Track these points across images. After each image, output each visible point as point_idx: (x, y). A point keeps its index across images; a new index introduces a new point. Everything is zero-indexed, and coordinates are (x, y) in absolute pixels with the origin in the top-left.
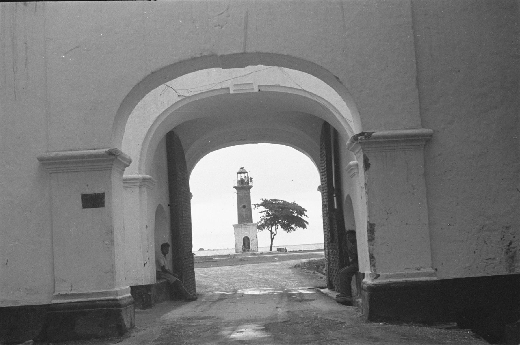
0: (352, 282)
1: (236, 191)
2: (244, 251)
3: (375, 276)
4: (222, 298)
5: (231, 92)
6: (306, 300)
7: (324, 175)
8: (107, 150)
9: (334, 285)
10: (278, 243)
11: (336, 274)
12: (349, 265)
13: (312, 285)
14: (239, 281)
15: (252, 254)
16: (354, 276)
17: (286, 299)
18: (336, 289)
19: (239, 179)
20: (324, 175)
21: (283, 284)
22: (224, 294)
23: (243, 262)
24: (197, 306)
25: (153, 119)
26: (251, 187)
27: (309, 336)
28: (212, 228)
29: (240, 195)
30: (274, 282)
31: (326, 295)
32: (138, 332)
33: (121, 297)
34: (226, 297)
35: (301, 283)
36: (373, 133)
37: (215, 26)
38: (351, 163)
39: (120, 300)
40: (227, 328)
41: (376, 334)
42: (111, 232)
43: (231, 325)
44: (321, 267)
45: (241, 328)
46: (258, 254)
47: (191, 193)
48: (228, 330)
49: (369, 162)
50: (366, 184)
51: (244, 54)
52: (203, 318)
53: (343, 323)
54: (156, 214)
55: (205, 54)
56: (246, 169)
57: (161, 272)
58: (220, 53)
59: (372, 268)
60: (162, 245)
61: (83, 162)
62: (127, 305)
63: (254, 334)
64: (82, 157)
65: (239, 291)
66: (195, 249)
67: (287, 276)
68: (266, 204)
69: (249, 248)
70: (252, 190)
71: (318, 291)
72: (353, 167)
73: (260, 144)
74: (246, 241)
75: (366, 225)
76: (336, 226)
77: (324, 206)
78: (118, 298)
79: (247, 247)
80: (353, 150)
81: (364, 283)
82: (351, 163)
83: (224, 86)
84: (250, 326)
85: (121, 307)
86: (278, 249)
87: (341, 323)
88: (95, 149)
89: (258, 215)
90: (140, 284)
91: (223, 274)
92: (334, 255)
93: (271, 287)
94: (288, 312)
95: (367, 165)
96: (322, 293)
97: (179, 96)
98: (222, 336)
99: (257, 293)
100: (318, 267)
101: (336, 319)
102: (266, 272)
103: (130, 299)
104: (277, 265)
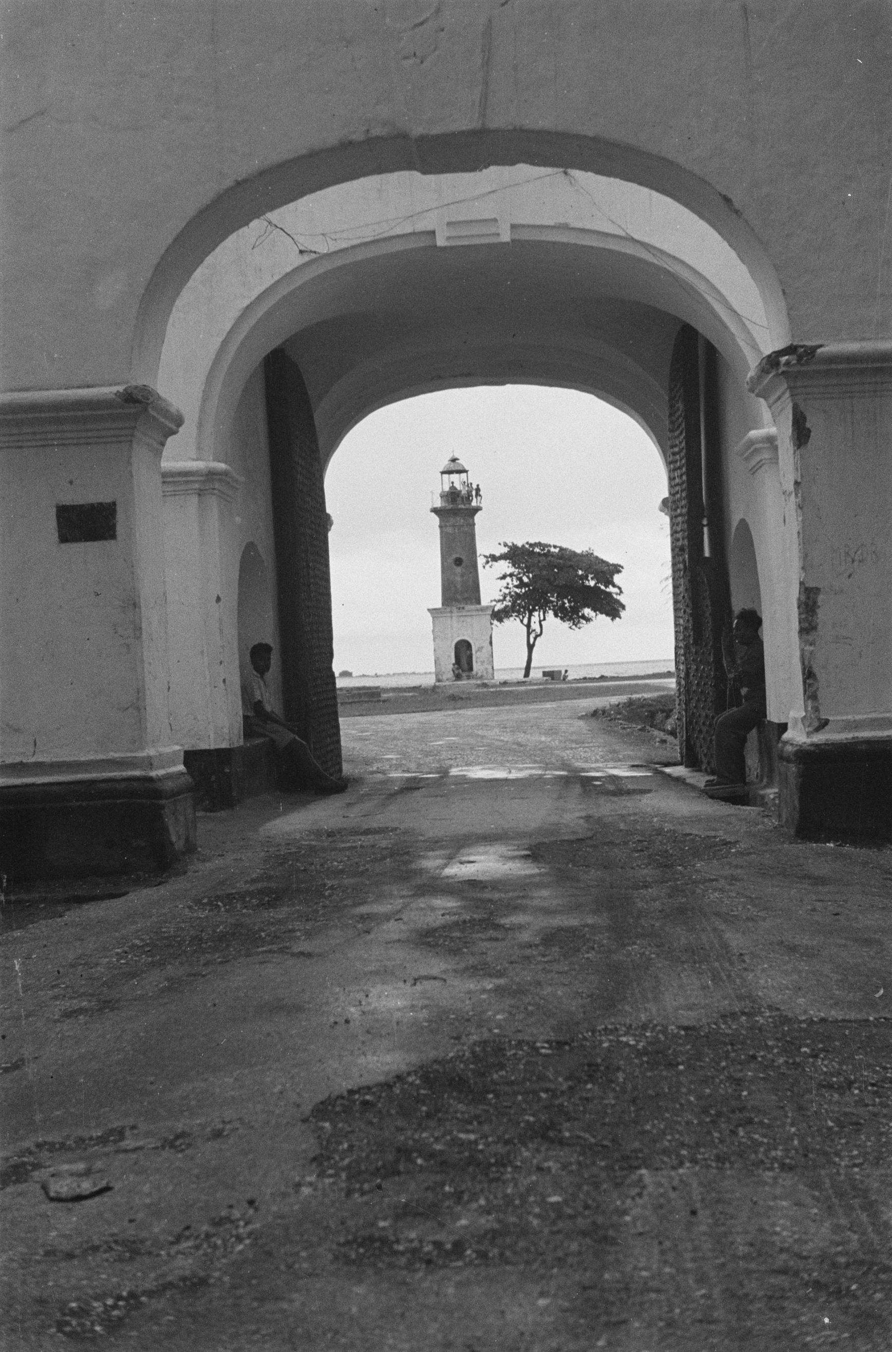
0: (748, 744)
1: (436, 520)
2: (458, 677)
3: (816, 724)
4: (412, 786)
5: (441, 242)
6: (629, 793)
7: (680, 468)
8: (121, 388)
9: (701, 756)
10: (543, 660)
11: (704, 729)
12: (739, 704)
13: (640, 758)
14: (451, 747)
15: (478, 686)
16: (754, 731)
17: (577, 789)
18: (704, 767)
19: (447, 488)
20: (680, 468)
21: (567, 754)
22: (415, 778)
23: (460, 703)
24: (349, 805)
25: (233, 314)
26: (478, 509)
27: (646, 871)
28: (381, 614)
29: (449, 530)
30: (541, 749)
31: (679, 780)
32: (204, 861)
33: (161, 772)
34: (421, 785)
35: (614, 751)
36: (821, 346)
37: (406, 58)
38: (753, 433)
39: (159, 779)
40: (431, 853)
41: (823, 868)
42: (135, 605)
43: (442, 848)
44: (660, 716)
45: (471, 854)
46: (494, 686)
47: (328, 516)
48: (436, 857)
49: (808, 425)
50: (797, 483)
51: (479, 133)
52: (367, 832)
53: (730, 843)
54: (242, 570)
55: (377, 132)
56: (463, 462)
57: (255, 717)
58: (417, 131)
59: (810, 703)
60: (260, 645)
61: (58, 421)
62: (178, 793)
63: (506, 867)
64: (57, 407)
65: (454, 772)
66: (337, 667)
67: (574, 737)
68: (515, 554)
69: (471, 669)
70: (478, 518)
71: (657, 772)
72: (758, 446)
73: (509, 387)
74: (463, 653)
75: (795, 592)
76: (708, 602)
77: (677, 551)
78: (153, 774)
79: (465, 666)
80: (764, 394)
81: (786, 743)
82: (753, 433)
83: (421, 226)
84: (491, 849)
85: (160, 798)
86: (545, 674)
87: (726, 843)
88: (88, 387)
89: (494, 583)
90: (203, 746)
91: (408, 732)
92: (701, 677)
93: (535, 762)
94: (588, 818)
95: (801, 434)
96: (669, 775)
97: (301, 252)
98: (421, 872)
99: (500, 774)
100: (652, 715)
101: (713, 834)
102: (519, 727)
103: (183, 780)
104: (547, 710)
